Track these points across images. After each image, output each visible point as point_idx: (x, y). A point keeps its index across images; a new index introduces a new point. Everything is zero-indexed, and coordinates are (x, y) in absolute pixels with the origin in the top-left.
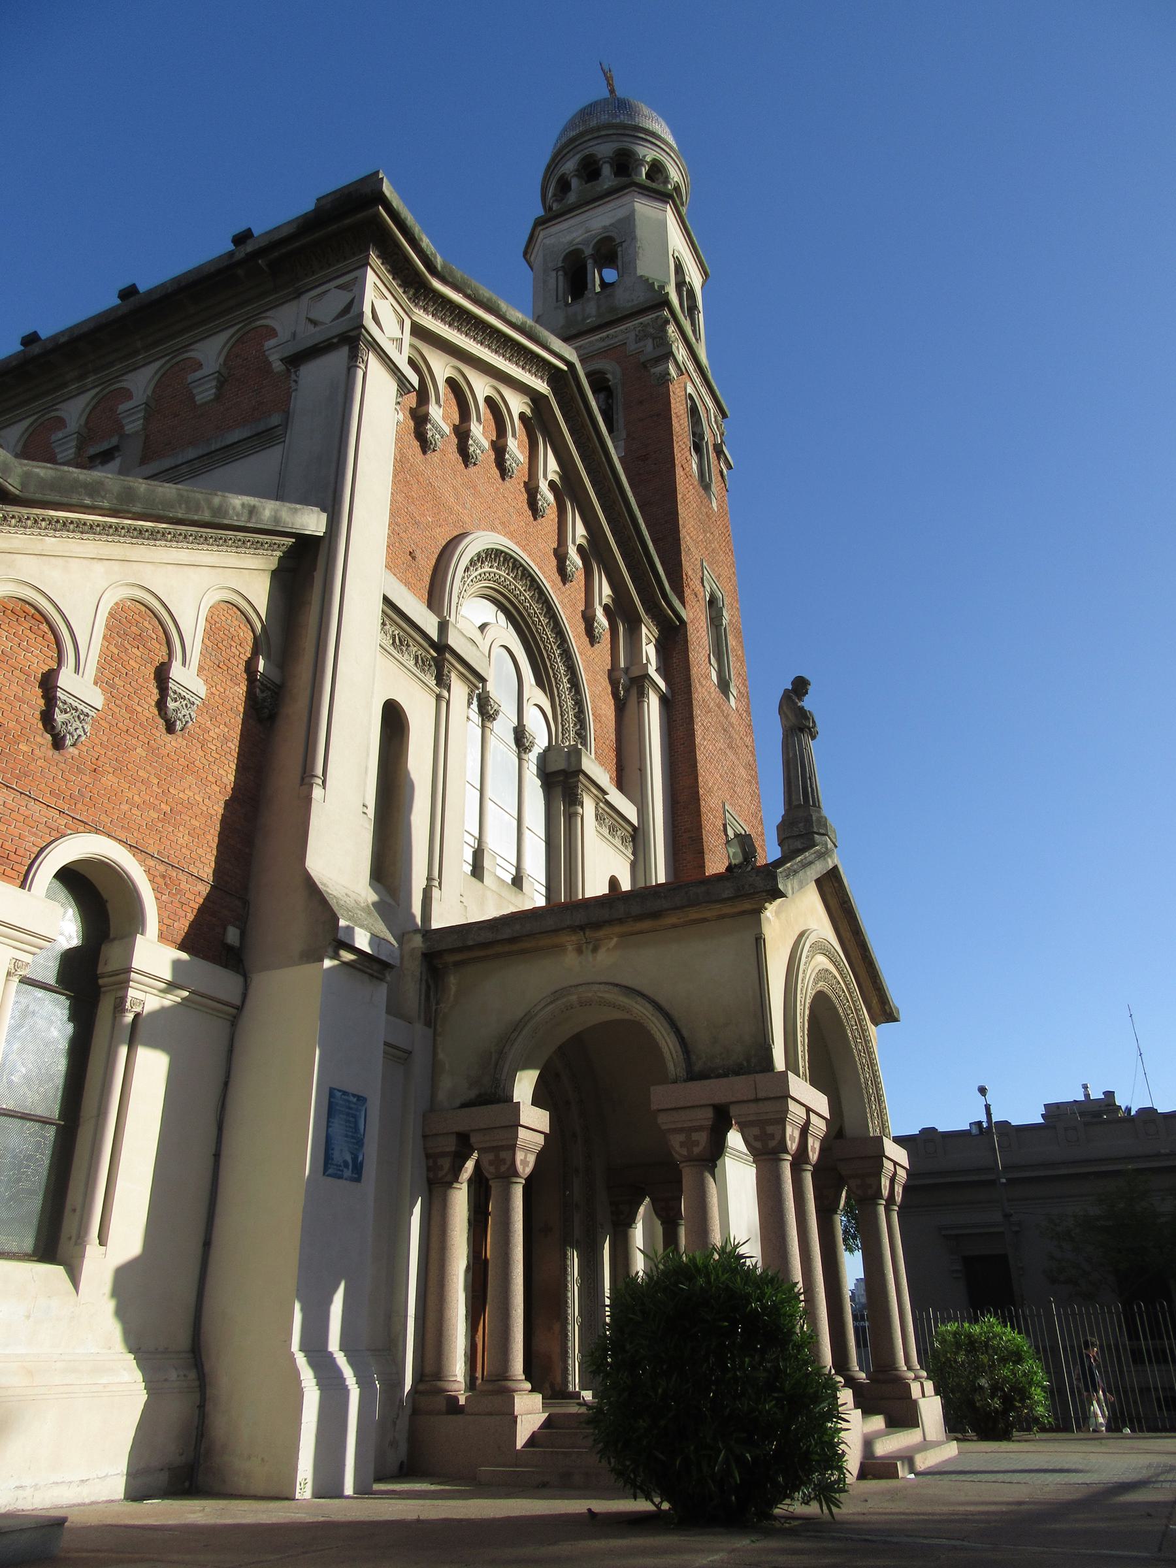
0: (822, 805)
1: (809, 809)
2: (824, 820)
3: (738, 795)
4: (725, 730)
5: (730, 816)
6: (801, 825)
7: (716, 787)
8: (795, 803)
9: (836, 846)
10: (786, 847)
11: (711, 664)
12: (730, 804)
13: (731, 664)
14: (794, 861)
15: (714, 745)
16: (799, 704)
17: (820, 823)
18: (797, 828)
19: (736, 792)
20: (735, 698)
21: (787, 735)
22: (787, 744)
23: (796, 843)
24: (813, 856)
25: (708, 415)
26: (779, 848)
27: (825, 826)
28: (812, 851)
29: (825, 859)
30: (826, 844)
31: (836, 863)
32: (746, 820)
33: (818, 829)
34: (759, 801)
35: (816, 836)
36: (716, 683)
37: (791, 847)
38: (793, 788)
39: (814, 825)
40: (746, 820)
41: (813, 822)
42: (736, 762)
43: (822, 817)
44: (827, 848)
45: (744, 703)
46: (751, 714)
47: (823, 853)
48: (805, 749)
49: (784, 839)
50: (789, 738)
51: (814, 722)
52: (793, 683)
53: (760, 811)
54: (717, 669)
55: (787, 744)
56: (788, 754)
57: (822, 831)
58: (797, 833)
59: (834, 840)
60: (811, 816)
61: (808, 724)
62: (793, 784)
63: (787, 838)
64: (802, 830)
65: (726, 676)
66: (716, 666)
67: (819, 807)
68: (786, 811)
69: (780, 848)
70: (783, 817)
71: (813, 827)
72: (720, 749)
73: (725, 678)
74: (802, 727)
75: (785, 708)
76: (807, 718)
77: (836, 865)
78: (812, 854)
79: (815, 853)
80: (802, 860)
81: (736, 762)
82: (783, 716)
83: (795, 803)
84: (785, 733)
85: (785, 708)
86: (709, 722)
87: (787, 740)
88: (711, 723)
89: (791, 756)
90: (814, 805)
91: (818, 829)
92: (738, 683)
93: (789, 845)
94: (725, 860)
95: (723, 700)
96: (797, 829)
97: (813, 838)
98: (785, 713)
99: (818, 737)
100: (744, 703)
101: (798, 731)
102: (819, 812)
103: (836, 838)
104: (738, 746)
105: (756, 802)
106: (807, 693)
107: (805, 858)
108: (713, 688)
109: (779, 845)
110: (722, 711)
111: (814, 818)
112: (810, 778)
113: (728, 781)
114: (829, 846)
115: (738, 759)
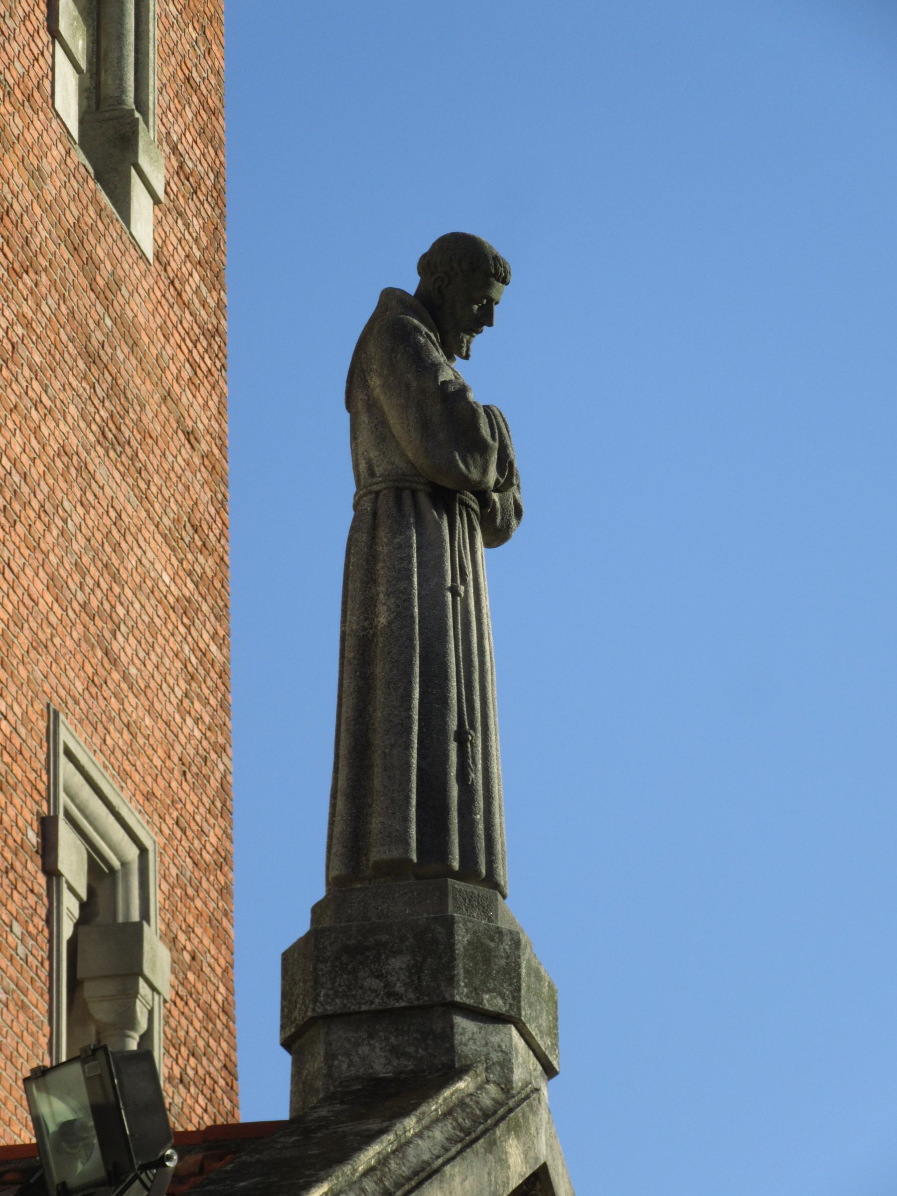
0: (507, 874)
1: (443, 893)
2: (506, 945)
3: (125, 677)
4: (92, 358)
5: (78, 779)
6: (398, 963)
7: (24, 640)
8: (378, 853)
9: (550, 1071)
10: (316, 1063)
11: (54, 33)
12: (93, 724)
13: (154, 31)
14: (347, 1169)
15: (36, 430)
16: (446, 375)
17: (487, 961)
18: (379, 976)
19: (114, 663)
20: (157, 201)
21: (375, 514)
22: (372, 558)
23: (364, 1050)
24: (438, 1134)
25: (51, 934)
26: (285, 1059)
27: (512, 974)
28: (435, 1106)
29: (492, 1145)
30: (506, 1065)
31: (543, 1152)
32: (149, 796)
33: (476, 991)
34: (224, 705)
35: (461, 1022)
36: (75, 133)
37: (343, 1066)
38: (378, 782)
39: (460, 971)
40: (149, 796)
41: (453, 958)
42: (134, 513)
43: (499, 931)
44: (506, 1086)
45: (196, 224)
46: (228, 277)
47: (486, 1116)
48: (455, 592)
49: (311, 1023)
50: (383, 534)
51: (506, 465)
52: (426, 265)
53: (221, 750)
54: (83, 65)
55: (372, 558)
56: (368, 607)
57: (492, 1002)
58: (377, 1003)
59: (543, 1043)
60: (449, 924)
61: (475, 475)
62: (377, 761)
63: (328, 1019)
64: (399, 988)
65: (122, 90)
66: (79, 45)
67: (492, 882)
68: (335, 884)
69: (348, 415)
70: (318, 911)
71: (451, 981)
72: (63, 450)
73: (120, 101)
74: (447, 483)
75: (375, 382)
76: (479, 448)
77: (544, 1168)
78: (436, 1121)
79: (448, 1113)
80: (383, 1161)
81: (134, 513)
82: (364, 418)
83: (378, 853)
84: (367, 505)
85: (375, 382)
86: (20, 316)
87: (373, 538)
88: (28, 325)
89: (382, 620)
90: (468, 871)
91: (476, 991)
92: (177, 129)
93: (330, 1057)
94: (33, 996)
95: (100, 212)
96: (377, 984)
97: (448, 1035)
98: (372, 406)
99: (519, 532)
100: (196, 224)
101: (424, 501)
102: (488, 908)
103: (553, 1032)
104: (146, 434)
105: (206, 703)
106: (485, 318)
107: (401, 1148)
108: (57, 152)
109: (287, 1044)
110: (90, 264)
111: (462, 938)
112: (462, 738)
113: (84, 606)
114: (518, 1076)
115: (143, 498)
